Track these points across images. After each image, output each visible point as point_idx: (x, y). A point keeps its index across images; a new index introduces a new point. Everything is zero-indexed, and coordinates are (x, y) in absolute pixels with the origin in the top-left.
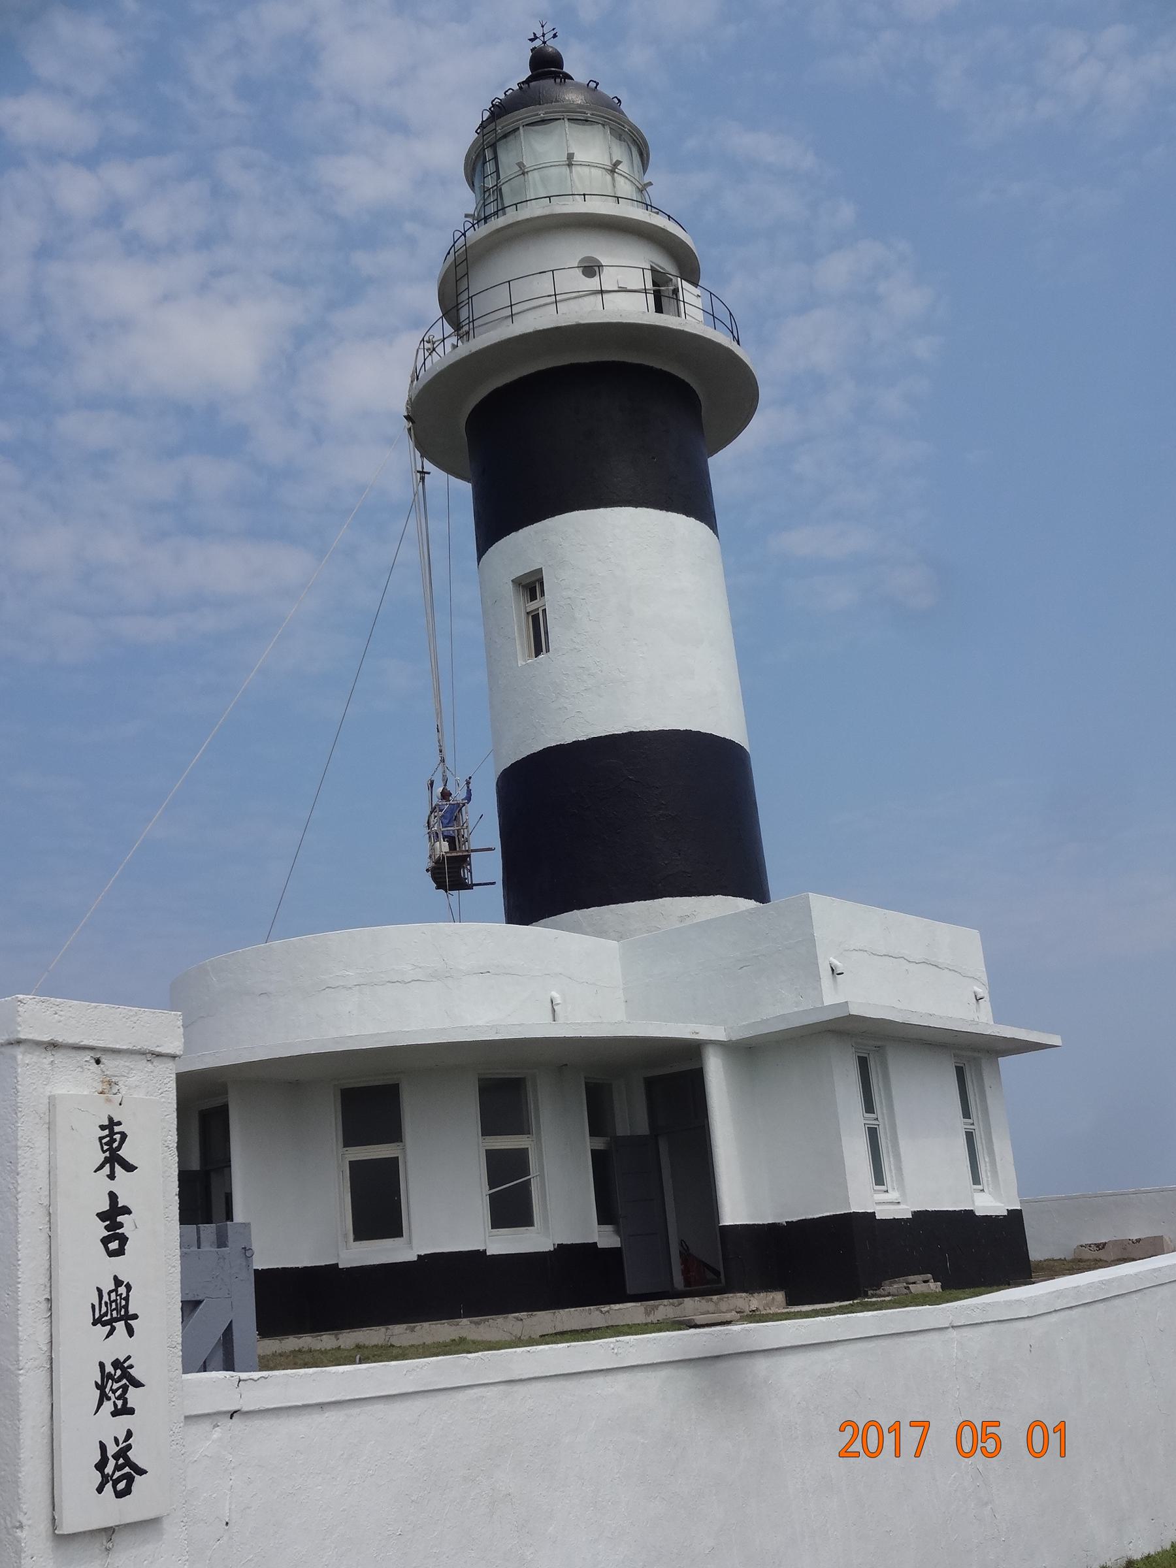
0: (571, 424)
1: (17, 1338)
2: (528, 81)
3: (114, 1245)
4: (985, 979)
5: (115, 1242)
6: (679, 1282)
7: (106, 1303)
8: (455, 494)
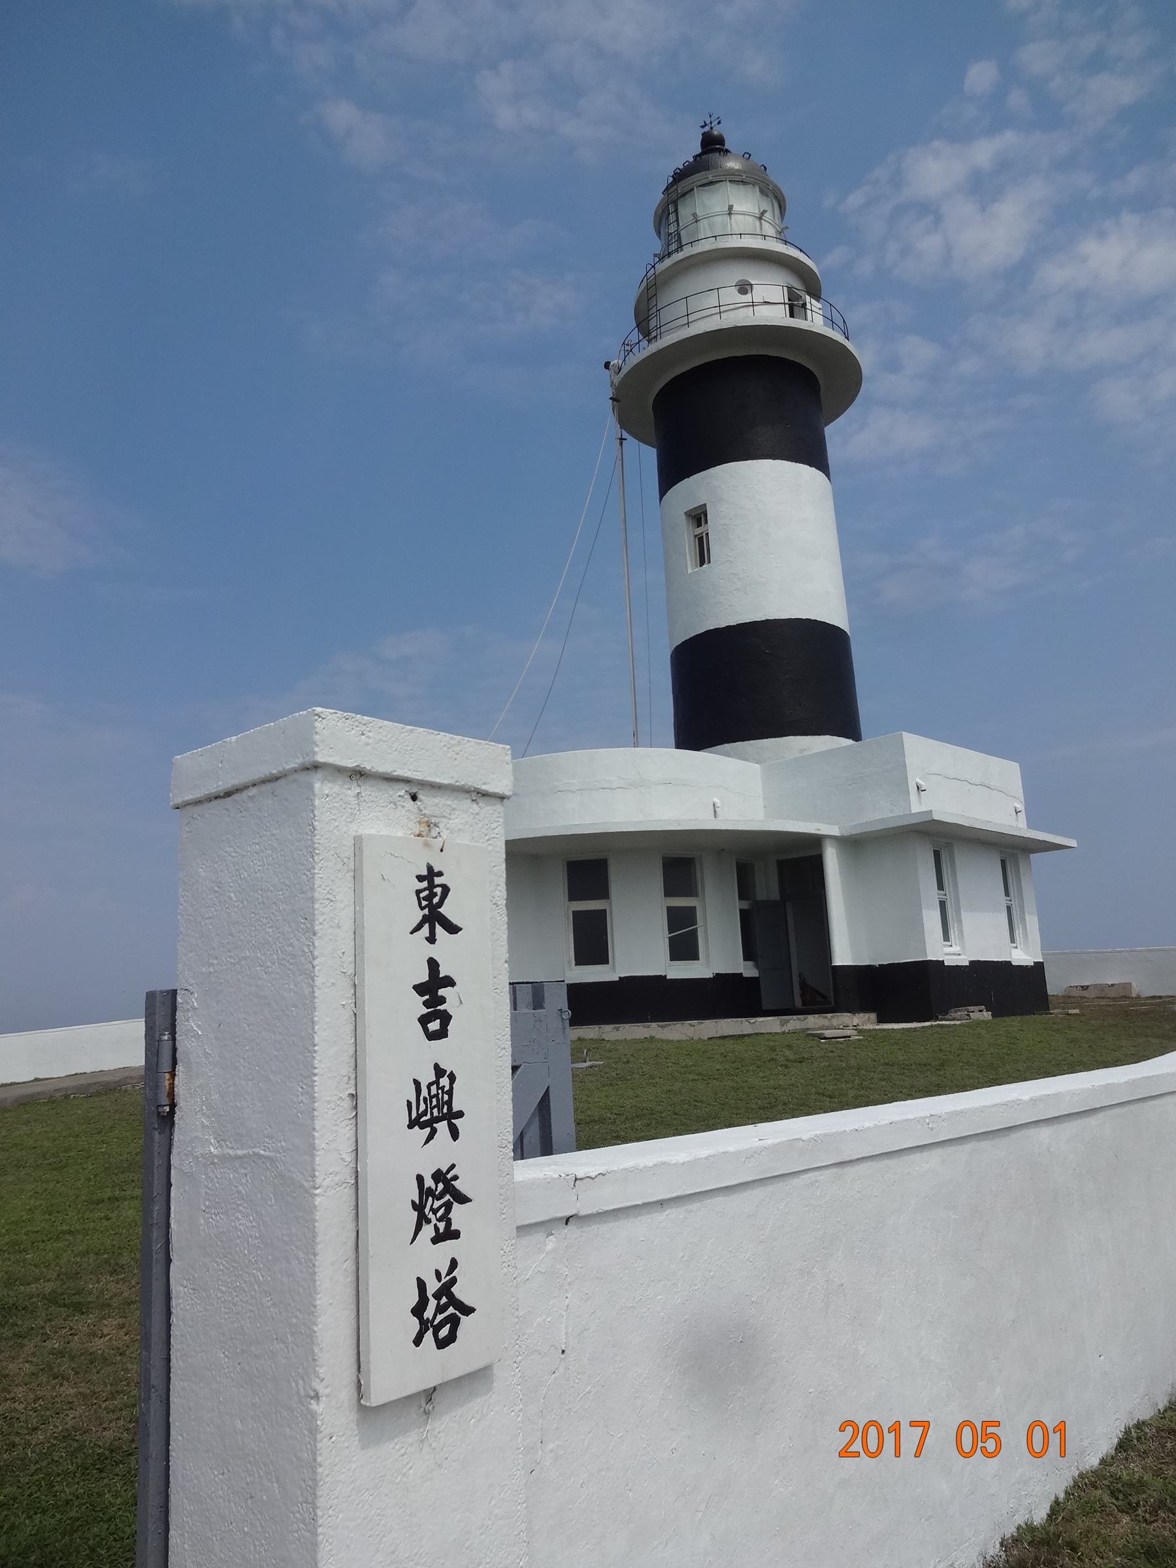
0: (730, 401)
1: (313, 1147)
2: (699, 155)
3: (434, 1026)
4: (1022, 798)
5: (436, 1021)
6: (798, 1003)
7: (425, 1099)
8: (645, 458)
